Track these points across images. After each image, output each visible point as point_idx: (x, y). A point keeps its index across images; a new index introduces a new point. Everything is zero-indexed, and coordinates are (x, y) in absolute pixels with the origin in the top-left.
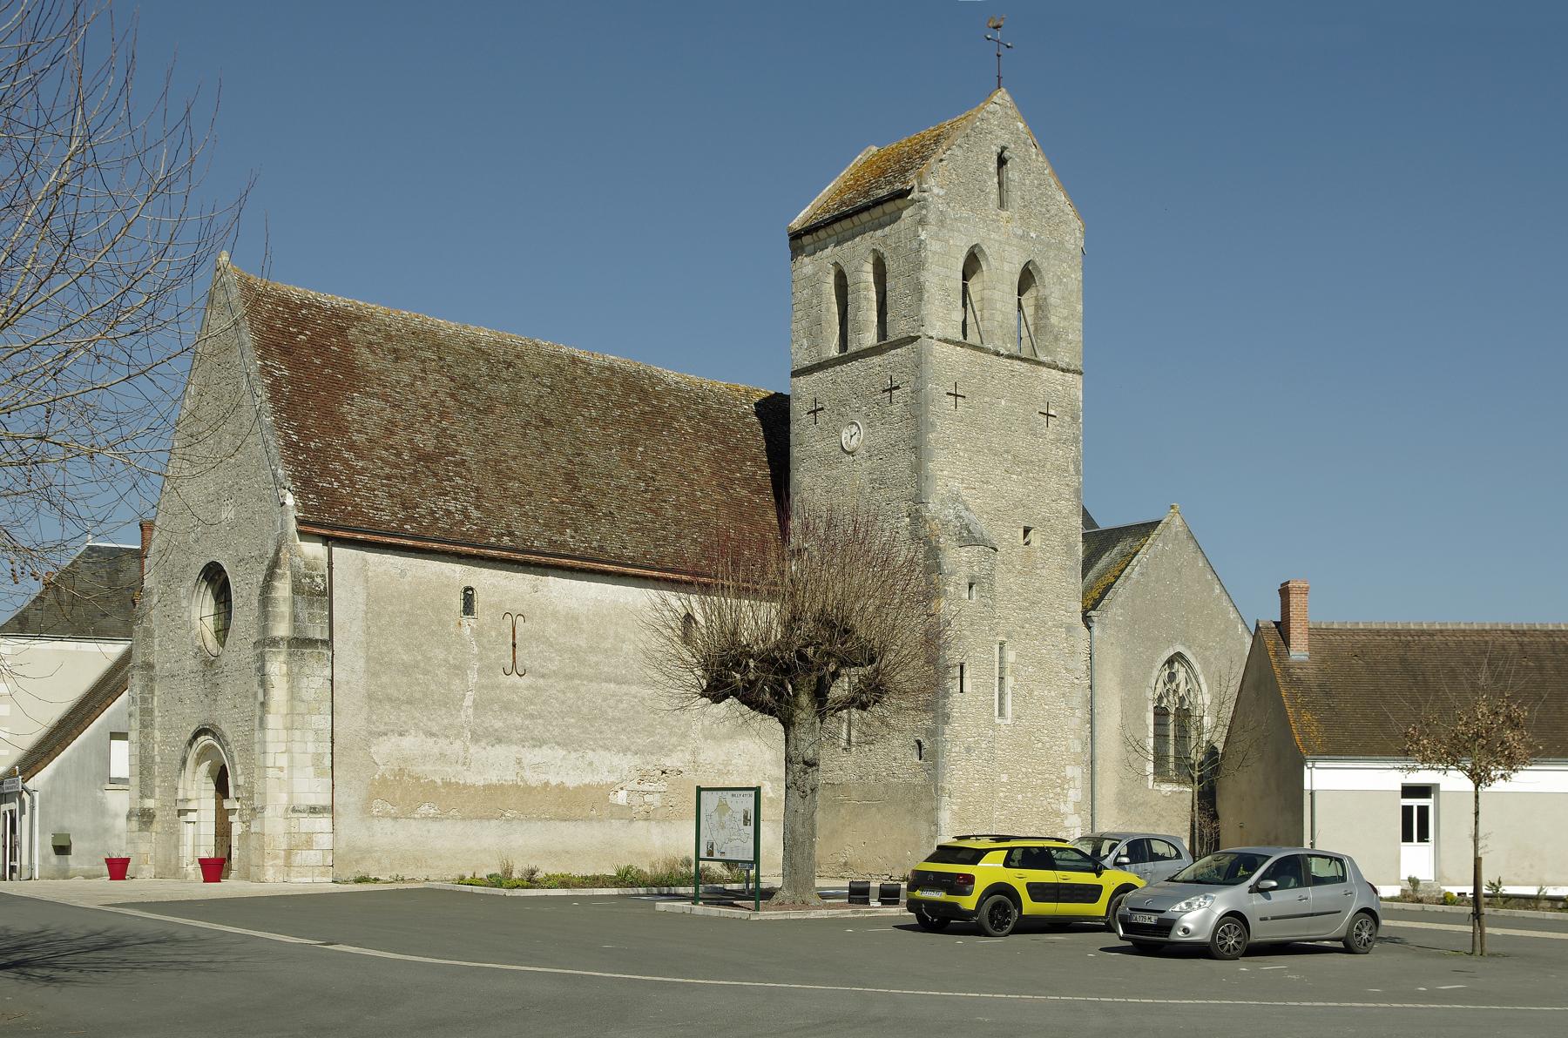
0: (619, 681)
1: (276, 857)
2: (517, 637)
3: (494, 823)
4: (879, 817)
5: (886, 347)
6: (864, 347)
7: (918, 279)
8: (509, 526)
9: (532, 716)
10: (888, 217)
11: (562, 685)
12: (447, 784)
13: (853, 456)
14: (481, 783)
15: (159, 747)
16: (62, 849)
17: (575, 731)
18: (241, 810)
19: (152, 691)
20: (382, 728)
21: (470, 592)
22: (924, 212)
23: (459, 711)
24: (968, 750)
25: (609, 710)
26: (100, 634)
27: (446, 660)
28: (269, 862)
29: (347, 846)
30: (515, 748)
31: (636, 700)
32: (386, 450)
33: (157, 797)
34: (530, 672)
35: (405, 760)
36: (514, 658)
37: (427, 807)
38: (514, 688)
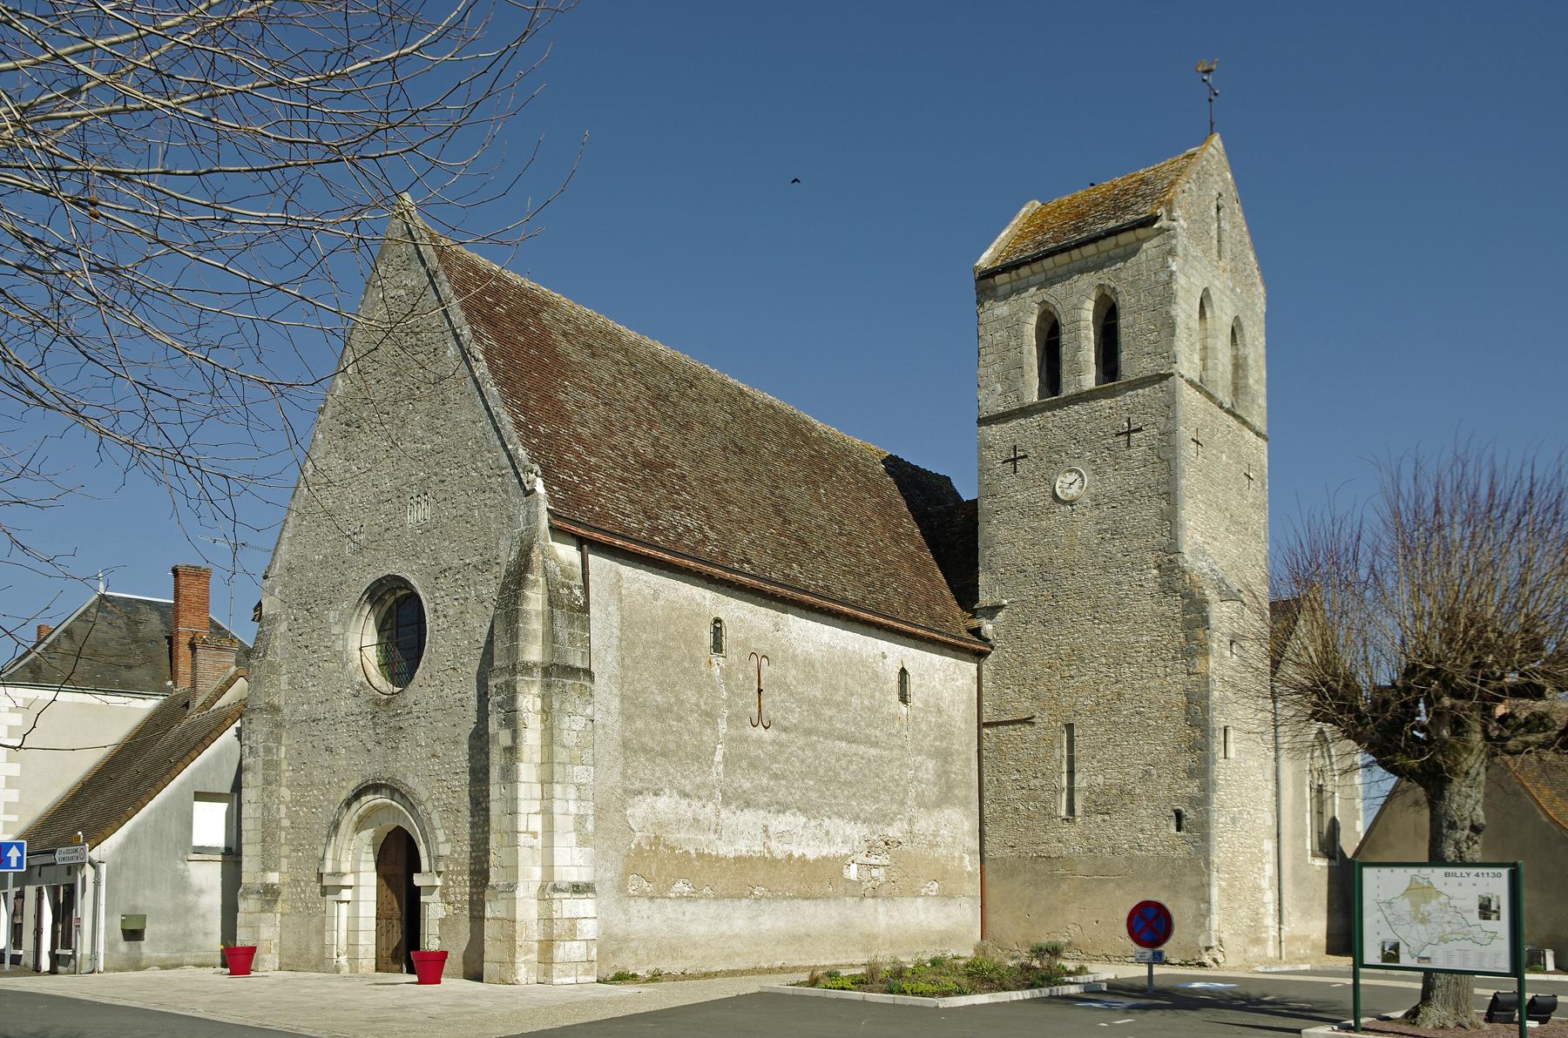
0: (851, 740)
1: (529, 951)
2: (762, 682)
3: (745, 902)
4: (1119, 893)
5: (1122, 386)
6: (1086, 389)
7: (1168, 313)
8: (744, 553)
9: (775, 777)
10: (1122, 249)
11: (801, 742)
12: (701, 856)
13: (1071, 505)
14: (731, 856)
15: (288, 808)
16: (133, 935)
17: (813, 795)
18: (446, 886)
19: (278, 740)
20: (638, 785)
21: (718, 625)
22: (1174, 241)
23: (710, 768)
24: (1234, 820)
25: (842, 772)
26: (126, 688)
27: (697, 705)
28: (520, 958)
29: (603, 934)
30: (762, 813)
31: (864, 762)
32: (611, 449)
33: (284, 868)
34: (774, 724)
35: (660, 825)
36: (760, 707)
37: (681, 884)
38: (759, 742)
